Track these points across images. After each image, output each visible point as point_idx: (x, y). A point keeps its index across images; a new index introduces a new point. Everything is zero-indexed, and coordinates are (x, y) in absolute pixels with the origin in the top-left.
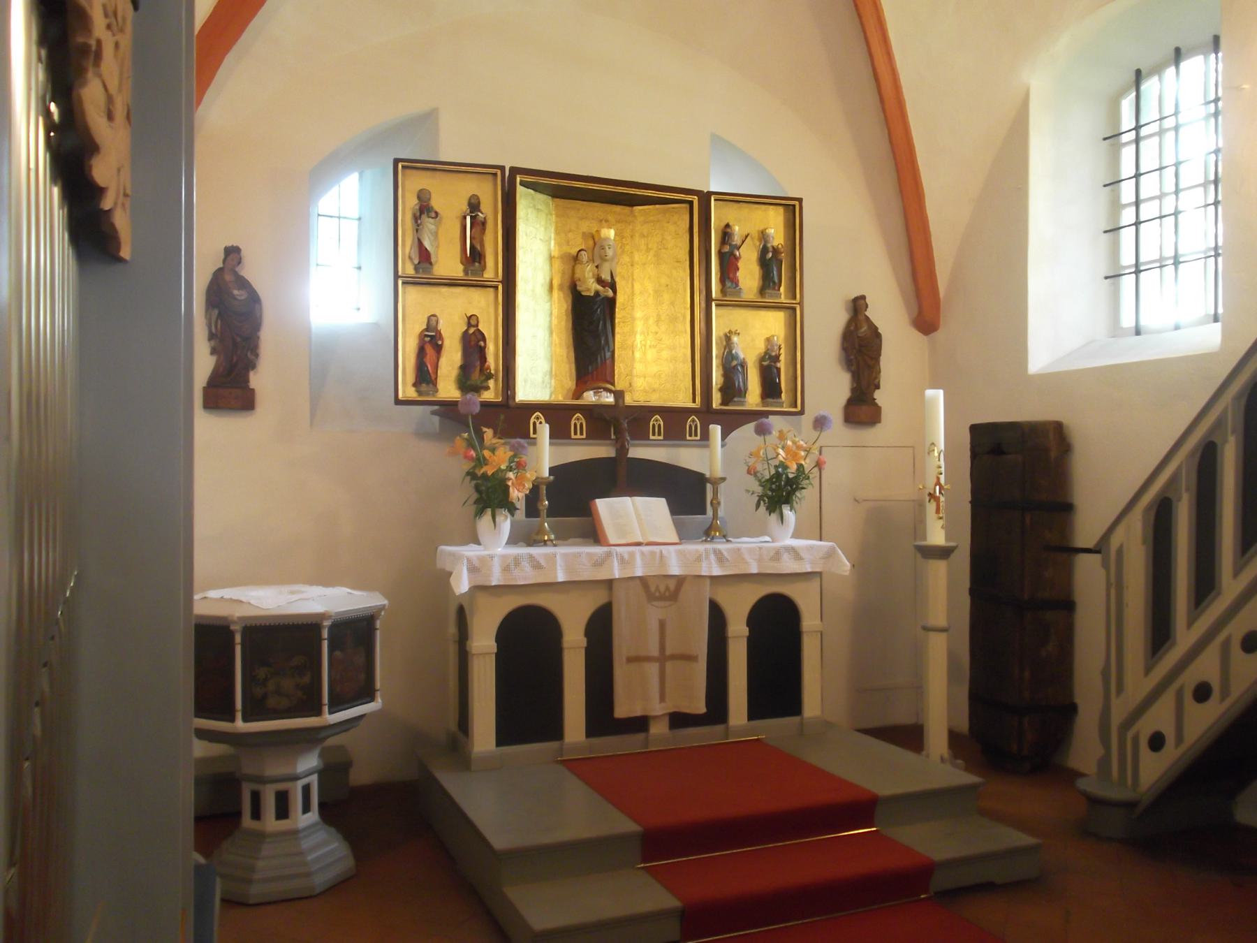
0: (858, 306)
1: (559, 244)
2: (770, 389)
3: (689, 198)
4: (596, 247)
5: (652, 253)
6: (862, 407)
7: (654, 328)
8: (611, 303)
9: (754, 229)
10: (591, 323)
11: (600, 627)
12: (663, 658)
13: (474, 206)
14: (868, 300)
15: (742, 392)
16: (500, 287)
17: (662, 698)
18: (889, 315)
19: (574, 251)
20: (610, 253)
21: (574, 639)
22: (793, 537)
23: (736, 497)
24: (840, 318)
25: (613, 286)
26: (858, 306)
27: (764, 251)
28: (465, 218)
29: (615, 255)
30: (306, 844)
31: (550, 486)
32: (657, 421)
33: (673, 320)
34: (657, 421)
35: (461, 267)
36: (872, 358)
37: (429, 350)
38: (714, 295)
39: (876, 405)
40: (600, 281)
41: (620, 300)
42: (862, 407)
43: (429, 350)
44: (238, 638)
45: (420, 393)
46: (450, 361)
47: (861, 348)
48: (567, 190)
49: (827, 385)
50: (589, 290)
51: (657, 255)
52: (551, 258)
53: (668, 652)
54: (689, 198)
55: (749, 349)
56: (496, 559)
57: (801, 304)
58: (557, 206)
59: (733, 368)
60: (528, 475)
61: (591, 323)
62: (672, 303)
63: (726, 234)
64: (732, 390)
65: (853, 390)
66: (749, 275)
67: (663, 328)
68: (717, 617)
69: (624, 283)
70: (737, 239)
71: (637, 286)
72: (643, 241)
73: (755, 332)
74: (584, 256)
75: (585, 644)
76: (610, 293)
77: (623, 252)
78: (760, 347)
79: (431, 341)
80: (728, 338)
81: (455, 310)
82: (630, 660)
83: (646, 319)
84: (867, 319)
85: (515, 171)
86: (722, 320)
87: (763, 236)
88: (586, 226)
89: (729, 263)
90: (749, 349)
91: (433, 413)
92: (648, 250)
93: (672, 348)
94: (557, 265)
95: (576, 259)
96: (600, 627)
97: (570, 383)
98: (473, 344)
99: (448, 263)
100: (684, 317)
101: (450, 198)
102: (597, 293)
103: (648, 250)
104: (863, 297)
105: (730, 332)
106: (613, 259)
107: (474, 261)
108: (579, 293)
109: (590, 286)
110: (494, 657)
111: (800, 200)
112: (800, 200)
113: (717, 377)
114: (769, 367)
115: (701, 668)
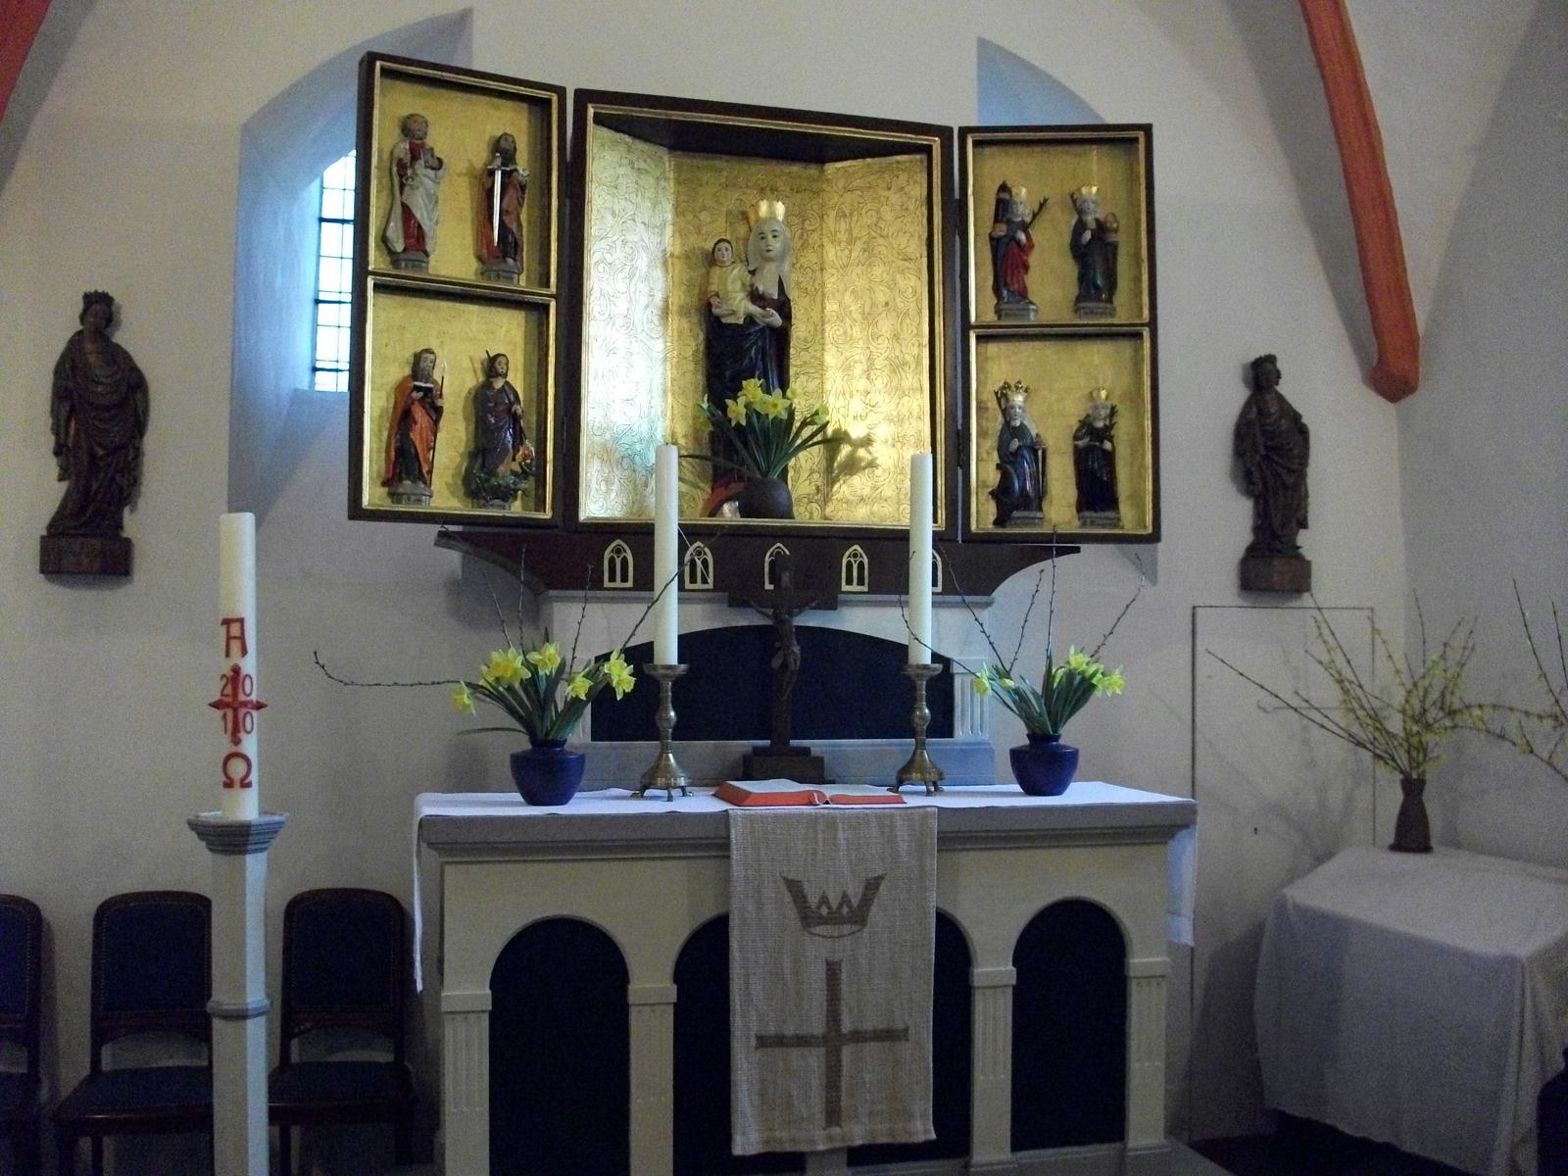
0: (1262, 374)
1: (681, 233)
2: (1097, 488)
3: (922, 140)
5: (859, 245)
6: (1273, 564)
7: (861, 384)
8: (780, 339)
9: (1055, 191)
11: (705, 960)
12: (833, 1040)
13: (503, 150)
14: (1280, 365)
15: (1033, 501)
16: (553, 304)
17: (833, 1115)
18: (1326, 390)
19: (709, 245)
20: (776, 245)
21: (652, 983)
22: (595, 113)
23: (859, 559)
24: (1235, 396)
25: (783, 306)
26: (1262, 374)
27: (1080, 227)
28: (491, 173)
31: (679, 682)
32: (855, 554)
33: (897, 367)
34: (855, 554)
35: (474, 264)
36: (1291, 471)
37: (420, 414)
38: (973, 319)
39: (1300, 558)
40: (756, 297)
41: (799, 331)
42: (1273, 564)
43: (420, 414)
45: (394, 496)
46: (449, 447)
47: (1270, 451)
48: (702, 137)
49: (1205, 512)
50: (734, 313)
51: (868, 250)
52: (665, 312)
53: (847, 1026)
54: (922, 140)
55: (1053, 425)
57: (1153, 324)
58: (678, 169)
59: (1019, 450)
60: (1540, 977)
61: (740, 351)
62: (896, 337)
63: (1003, 206)
65: (1257, 529)
66: (1051, 281)
67: (879, 383)
68: (952, 945)
69: (806, 301)
70: (1023, 211)
71: (831, 307)
72: (843, 226)
73: (1053, 390)
75: (674, 998)
76: (776, 320)
77: (805, 245)
78: (1073, 412)
79: (418, 397)
80: (1002, 396)
81: (468, 343)
82: (763, 1042)
83: (847, 368)
84: (1281, 398)
86: (993, 367)
87: (1077, 205)
88: (732, 201)
89: (1009, 259)
90: (1053, 425)
92: (851, 241)
93: (900, 421)
95: (711, 259)
96: (705, 960)
97: (703, 494)
98: (491, 405)
99: (453, 255)
100: (919, 363)
101: (464, 133)
102: (750, 319)
103: (851, 241)
104: (1270, 359)
105: (1007, 386)
106: (782, 258)
107: (505, 255)
108: (717, 318)
109: (737, 306)
110: (485, 1021)
111: (1147, 129)
112: (1147, 129)
113: (983, 469)
114: (1089, 449)
115: (920, 1053)
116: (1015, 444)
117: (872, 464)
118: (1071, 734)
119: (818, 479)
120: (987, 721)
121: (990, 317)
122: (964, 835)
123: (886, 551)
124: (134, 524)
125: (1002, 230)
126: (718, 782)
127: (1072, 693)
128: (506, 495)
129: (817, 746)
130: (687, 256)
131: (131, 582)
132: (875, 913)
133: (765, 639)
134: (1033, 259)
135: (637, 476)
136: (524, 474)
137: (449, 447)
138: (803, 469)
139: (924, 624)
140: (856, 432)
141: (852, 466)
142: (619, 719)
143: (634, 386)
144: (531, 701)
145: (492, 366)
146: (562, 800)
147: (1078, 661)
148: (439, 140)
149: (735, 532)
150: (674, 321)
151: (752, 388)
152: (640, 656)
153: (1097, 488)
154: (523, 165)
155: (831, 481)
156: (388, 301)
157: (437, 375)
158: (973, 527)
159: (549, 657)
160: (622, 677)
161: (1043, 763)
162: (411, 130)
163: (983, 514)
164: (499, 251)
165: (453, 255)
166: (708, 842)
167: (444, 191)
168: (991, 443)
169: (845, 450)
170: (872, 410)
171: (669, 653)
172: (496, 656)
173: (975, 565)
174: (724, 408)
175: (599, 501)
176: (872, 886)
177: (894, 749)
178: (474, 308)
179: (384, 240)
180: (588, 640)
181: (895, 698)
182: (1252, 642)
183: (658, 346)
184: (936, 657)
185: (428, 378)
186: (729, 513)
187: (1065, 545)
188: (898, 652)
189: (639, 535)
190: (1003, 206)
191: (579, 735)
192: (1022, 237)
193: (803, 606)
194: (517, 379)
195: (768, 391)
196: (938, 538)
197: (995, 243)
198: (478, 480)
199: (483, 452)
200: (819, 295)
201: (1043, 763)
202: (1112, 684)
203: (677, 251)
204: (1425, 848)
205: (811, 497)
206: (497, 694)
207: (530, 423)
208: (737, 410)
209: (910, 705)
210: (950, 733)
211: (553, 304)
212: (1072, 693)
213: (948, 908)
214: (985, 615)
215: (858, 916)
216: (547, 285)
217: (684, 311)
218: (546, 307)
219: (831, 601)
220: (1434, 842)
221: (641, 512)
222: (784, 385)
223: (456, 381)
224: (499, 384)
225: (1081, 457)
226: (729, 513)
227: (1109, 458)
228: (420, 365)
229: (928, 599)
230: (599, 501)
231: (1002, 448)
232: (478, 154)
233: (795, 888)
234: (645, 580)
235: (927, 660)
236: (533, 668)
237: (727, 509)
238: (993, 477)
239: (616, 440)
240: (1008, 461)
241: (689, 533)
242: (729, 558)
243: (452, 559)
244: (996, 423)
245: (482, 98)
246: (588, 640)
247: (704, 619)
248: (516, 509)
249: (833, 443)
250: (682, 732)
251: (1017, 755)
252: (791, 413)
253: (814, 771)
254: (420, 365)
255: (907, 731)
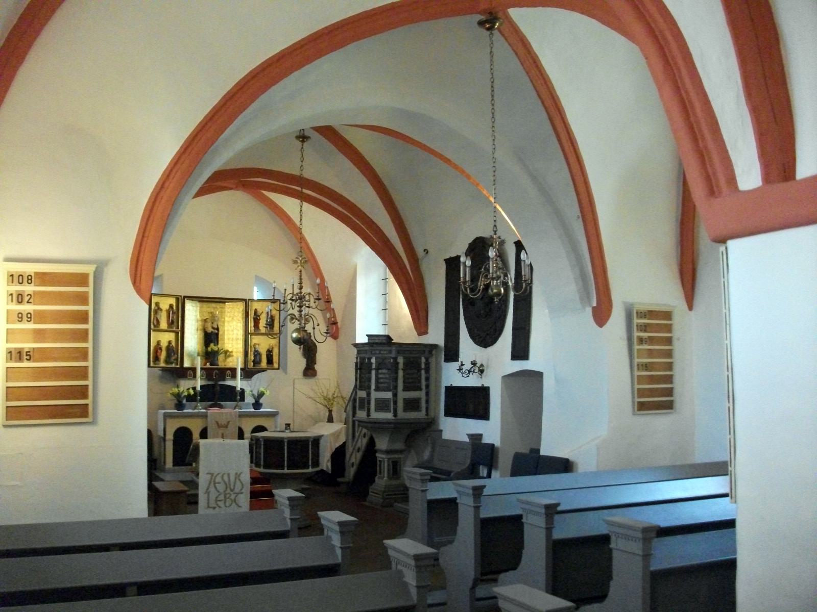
2: (270, 361)
4: (213, 318)
6: (310, 371)
8: (217, 335)
10: (211, 337)
13: (171, 306)
15: (260, 362)
16: (180, 333)
25: (218, 329)
29: (218, 319)
30: (495, 282)
31: (200, 393)
32: (229, 372)
35: (167, 325)
37: (159, 351)
41: (220, 333)
42: (310, 371)
44: (286, 444)
46: (163, 355)
52: (197, 330)
55: (263, 351)
56: (9, 289)
59: (257, 354)
61: (211, 337)
64: (257, 362)
69: (222, 327)
70: (259, 313)
73: (263, 343)
74: (208, 321)
76: (216, 332)
81: (166, 338)
85: (185, 297)
86: (255, 340)
90: (263, 351)
91: (160, 370)
94: (200, 323)
95: (205, 321)
97: (204, 361)
98: (169, 348)
99: (164, 325)
102: (212, 332)
109: (210, 330)
110: (172, 442)
113: (251, 357)
116: (256, 353)
117: (233, 356)
118: (261, 401)
119: (224, 358)
120: (249, 400)
121: (253, 331)
122: (242, 415)
123: (233, 371)
124: (317, 367)
125: (255, 317)
126: (205, 409)
127: (261, 395)
128: (172, 363)
129: (222, 403)
130: (202, 320)
131: (577, 464)
132: (229, 426)
133: (213, 386)
134: (261, 321)
135: (192, 357)
136: (174, 360)
137: (163, 355)
138: (221, 358)
139: (239, 383)
140: (230, 350)
141: (229, 356)
142: (191, 398)
143: (192, 342)
144: (178, 396)
145: (170, 342)
146: (182, 410)
147: (262, 389)
148: (161, 306)
149: (209, 368)
150: (199, 332)
151: (212, 345)
152: (194, 389)
153: (270, 361)
154: (174, 308)
155: (226, 359)
156: (154, 333)
157: (161, 344)
158: (249, 367)
159: (181, 389)
160: (192, 392)
161: (257, 405)
162: (157, 304)
163: (251, 365)
164: (171, 324)
165: (164, 325)
166: (204, 416)
167: (162, 314)
168: (252, 353)
169: (228, 353)
170: (233, 338)
171: (199, 388)
172: (173, 389)
173: (248, 374)
174: (207, 349)
175: (187, 364)
176: (229, 422)
177: (234, 403)
178: (167, 333)
179: (153, 323)
180: (185, 386)
181: (235, 396)
182: (305, 386)
183: (196, 336)
184: (241, 389)
185: (160, 345)
186: (208, 365)
187: (264, 370)
188: (234, 388)
189: (194, 370)
190: (256, 311)
191: (184, 402)
192: (258, 318)
193: (220, 381)
194: (173, 344)
195: (215, 345)
196: (241, 369)
197: (254, 319)
198: (167, 361)
199: (169, 356)
200: (224, 326)
201: (257, 405)
202: (267, 393)
203: (200, 319)
204: (332, 422)
205: (222, 363)
206: (173, 394)
207: (176, 351)
208: (209, 349)
209: (236, 396)
210: (244, 401)
211: (180, 333)
212: (261, 395)
213: (240, 426)
214: (249, 382)
215: (226, 426)
216: (178, 329)
217: (201, 330)
218: (178, 333)
219: (224, 380)
220: (334, 420)
221: (193, 365)
222: (218, 344)
223: (164, 344)
224: (171, 345)
225: (267, 356)
226: (208, 365)
227: (272, 356)
228: (158, 343)
229: (239, 379)
230: (187, 364)
231: (254, 353)
232: (167, 307)
233: (217, 423)
234: (195, 376)
235: (239, 389)
236: (179, 390)
237: (208, 364)
238: (253, 358)
239: (189, 353)
240: (255, 356)
241: (202, 369)
242: (208, 373)
243: (160, 372)
244: (253, 350)
245: (171, 298)
246: (185, 386)
247: (204, 383)
248: (173, 365)
249: (226, 352)
250: (201, 401)
251: (253, 404)
252: (219, 349)
253: (221, 407)
254: (158, 343)
255: (235, 400)
